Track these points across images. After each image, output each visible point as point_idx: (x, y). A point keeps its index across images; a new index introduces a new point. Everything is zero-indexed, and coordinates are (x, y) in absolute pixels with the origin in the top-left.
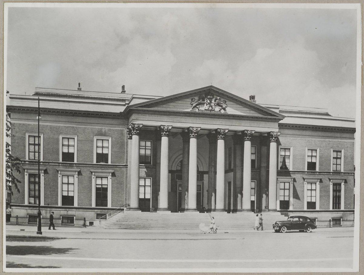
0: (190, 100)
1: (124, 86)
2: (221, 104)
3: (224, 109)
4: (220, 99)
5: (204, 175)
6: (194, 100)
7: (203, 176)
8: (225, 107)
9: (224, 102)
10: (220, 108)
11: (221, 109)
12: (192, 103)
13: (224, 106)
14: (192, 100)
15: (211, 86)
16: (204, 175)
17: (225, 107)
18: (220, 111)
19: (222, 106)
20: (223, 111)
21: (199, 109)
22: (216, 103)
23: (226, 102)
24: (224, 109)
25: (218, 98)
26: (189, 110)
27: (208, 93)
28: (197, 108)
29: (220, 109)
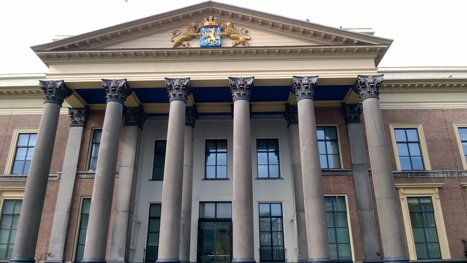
0: (172, 35)
12: (173, 39)
15: (210, 3)
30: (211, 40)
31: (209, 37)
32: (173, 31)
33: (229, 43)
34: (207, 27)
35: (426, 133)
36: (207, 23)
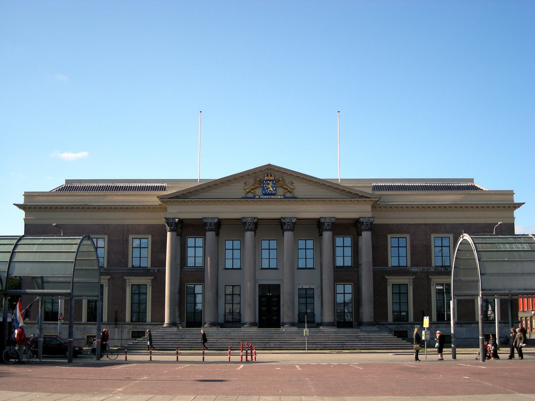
0: (243, 185)
14: (245, 183)
15: (269, 165)
30: (270, 190)
31: (269, 188)
32: (244, 181)
34: (267, 180)
35: (412, 241)
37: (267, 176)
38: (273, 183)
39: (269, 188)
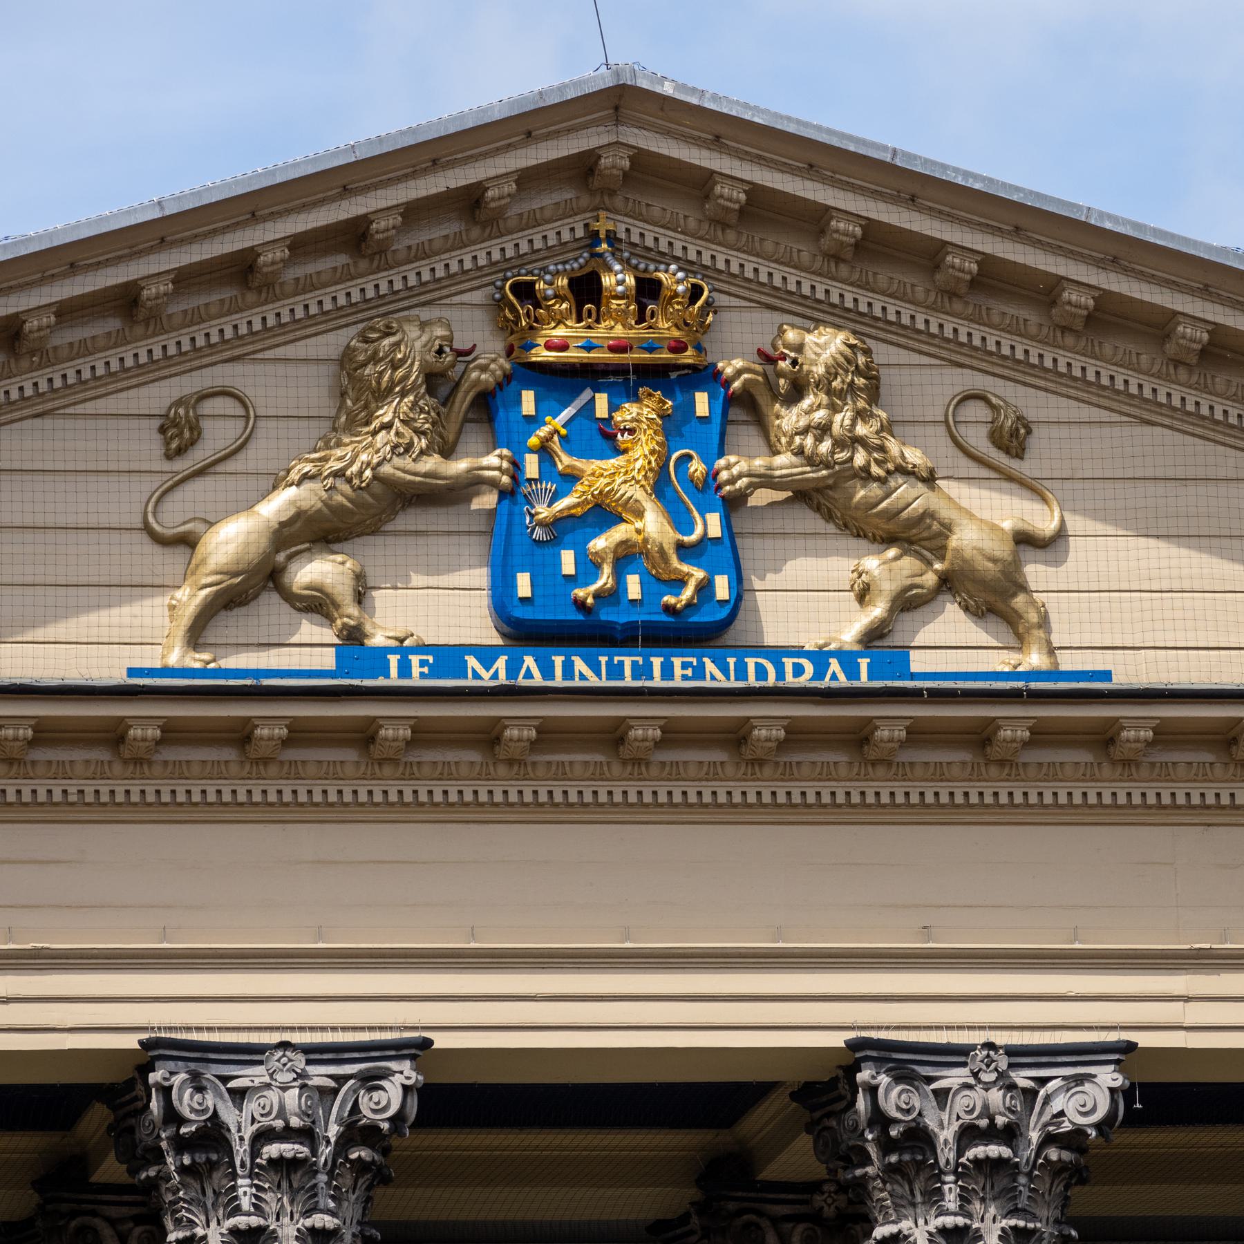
0: (145, 446)
1: (759, 350)
2: (904, 471)
3: (994, 596)
4: (863, 384)
5: (519, 575)
6: (218, 434)
7: (520, 395)
8: (1003, 550)
9: (977, 438)
10: (886, 568)
11: (908, 603)
13: (983, 515)
14: (179, 433)
15: (621, 100)
16: (519, 575)
17: (1003, 550)
18: (874, 636)
19: (917, 535)
20: (951, 645)
21: (353, 637)
22: (784, 462)
23: (1013, 439)
24: (994, 596)
25: (825, 346)
26: (132, 636)
27: (598, 242)
28: (317, 604)
29: (877, 611)
32: (160, 396)
33: (812, 604)
34: (564, 380)
36: (564, 337)
37: (586, 292)
38: (674, 426)
39: (603, 513)
